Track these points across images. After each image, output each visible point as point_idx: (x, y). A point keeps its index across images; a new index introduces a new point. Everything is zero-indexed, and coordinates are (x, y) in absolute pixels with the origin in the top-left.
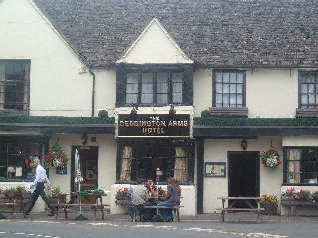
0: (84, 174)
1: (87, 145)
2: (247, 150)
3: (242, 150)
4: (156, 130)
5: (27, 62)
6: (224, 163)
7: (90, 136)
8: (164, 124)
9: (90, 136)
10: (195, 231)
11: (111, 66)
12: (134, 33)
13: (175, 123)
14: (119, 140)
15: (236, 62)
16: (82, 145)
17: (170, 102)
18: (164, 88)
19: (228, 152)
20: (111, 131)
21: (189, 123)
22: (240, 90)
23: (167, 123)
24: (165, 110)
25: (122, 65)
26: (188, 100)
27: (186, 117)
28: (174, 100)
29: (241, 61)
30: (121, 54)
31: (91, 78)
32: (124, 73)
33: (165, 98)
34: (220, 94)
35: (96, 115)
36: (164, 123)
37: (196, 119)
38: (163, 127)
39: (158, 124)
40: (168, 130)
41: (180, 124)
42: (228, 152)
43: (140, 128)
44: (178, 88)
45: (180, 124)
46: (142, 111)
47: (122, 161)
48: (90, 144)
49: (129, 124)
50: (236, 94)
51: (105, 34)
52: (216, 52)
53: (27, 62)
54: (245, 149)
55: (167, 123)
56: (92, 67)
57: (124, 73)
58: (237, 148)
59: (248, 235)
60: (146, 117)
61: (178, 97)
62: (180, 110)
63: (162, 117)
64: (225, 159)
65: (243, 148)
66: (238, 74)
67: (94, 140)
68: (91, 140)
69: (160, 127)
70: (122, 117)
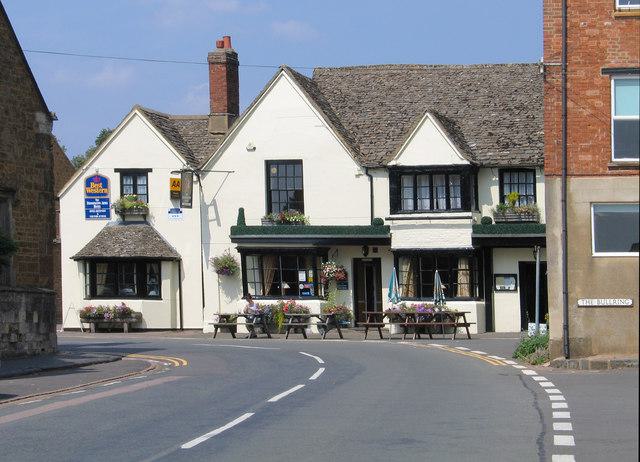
0: (444, 281)
6: (515, 276)
7: (371, 247)
9: (371, 247)
10: (437, 348)
11: (382, 167)
12: (403, 132)
15: (523, 160)
25: (395, 167)
29: (530, 159)
30: (391, 153)
32: (397, 175)
42: (520, 262)
48: (372, 255)
51: (390, 125)
52: (506, 146)
53: (299, 162)
56: (369, 170)
57: (397, 175)
59: (452, 350)
64: (516, 271)
67: (375, 250)
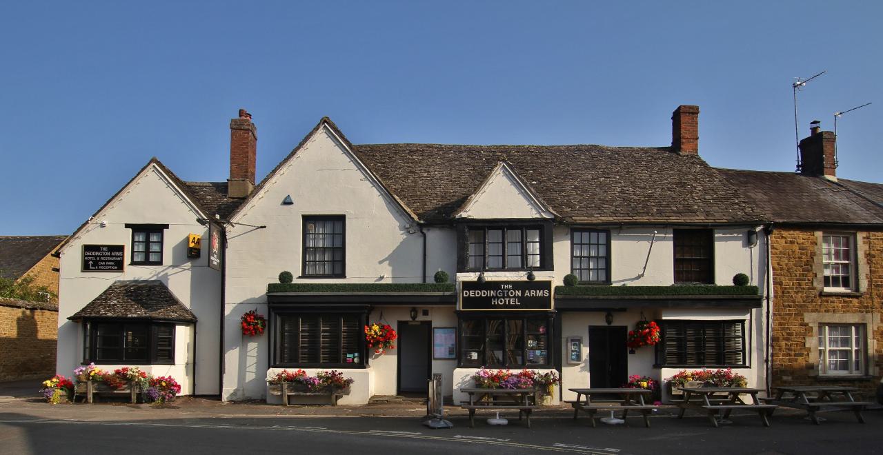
1: (417, 319)
2: (612, 325)
3: (606, 324)
4: (509, 301)
5: (82, 271)
8: (520, 295)
13: (533, 293)
14: (459, 313)
16: (411, 320)
17: (524, 266)
18: (513, 249)
19: (590, 326)
20: (451, 300)
21: (550, 293)
22: (602, 253)
23: (523, 293)
24: (521, 276)
26: (547, 264)
27: (546, 285)
28: (530, 264)
31: (421, 240)
33: (518, 262)
34: (577, 257)
35: (430, 280)
36: (519, 293)
37: (557, 288)
38: (518, 297)
39: (512, 293)
40: (524, 301)
41: (539, 293)
43: (489, 299)
44: (535, 248)
45: (539, 293)
46: (489, 276)
47: (187, 325)
49: (475, 294)
50: (597, 258)
54: (609, 322)
55: (523, 293)
58: (600, 321)
60: (495, 285)
61: (536, 261)
62: (540, 276)
63: (516, 285)
65: (411, 317)
66: (591, 234)
68: (422, 313)
69: (515, 297)
70: (467, 285)
